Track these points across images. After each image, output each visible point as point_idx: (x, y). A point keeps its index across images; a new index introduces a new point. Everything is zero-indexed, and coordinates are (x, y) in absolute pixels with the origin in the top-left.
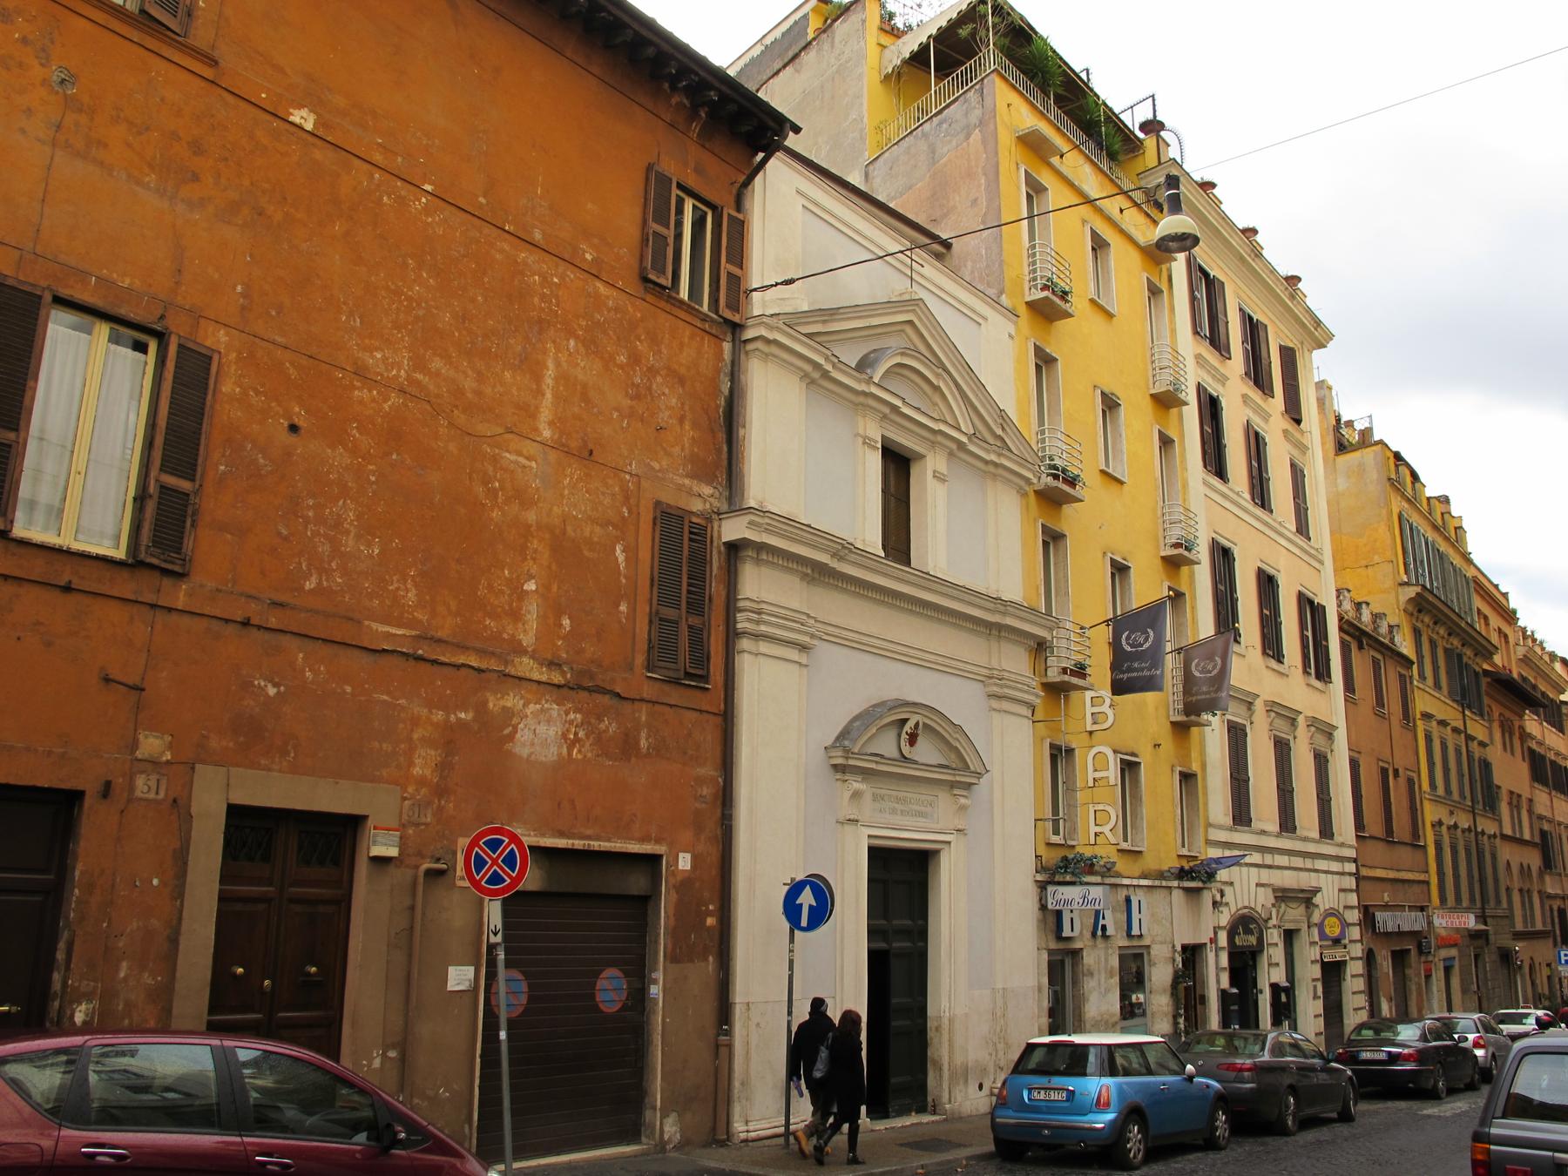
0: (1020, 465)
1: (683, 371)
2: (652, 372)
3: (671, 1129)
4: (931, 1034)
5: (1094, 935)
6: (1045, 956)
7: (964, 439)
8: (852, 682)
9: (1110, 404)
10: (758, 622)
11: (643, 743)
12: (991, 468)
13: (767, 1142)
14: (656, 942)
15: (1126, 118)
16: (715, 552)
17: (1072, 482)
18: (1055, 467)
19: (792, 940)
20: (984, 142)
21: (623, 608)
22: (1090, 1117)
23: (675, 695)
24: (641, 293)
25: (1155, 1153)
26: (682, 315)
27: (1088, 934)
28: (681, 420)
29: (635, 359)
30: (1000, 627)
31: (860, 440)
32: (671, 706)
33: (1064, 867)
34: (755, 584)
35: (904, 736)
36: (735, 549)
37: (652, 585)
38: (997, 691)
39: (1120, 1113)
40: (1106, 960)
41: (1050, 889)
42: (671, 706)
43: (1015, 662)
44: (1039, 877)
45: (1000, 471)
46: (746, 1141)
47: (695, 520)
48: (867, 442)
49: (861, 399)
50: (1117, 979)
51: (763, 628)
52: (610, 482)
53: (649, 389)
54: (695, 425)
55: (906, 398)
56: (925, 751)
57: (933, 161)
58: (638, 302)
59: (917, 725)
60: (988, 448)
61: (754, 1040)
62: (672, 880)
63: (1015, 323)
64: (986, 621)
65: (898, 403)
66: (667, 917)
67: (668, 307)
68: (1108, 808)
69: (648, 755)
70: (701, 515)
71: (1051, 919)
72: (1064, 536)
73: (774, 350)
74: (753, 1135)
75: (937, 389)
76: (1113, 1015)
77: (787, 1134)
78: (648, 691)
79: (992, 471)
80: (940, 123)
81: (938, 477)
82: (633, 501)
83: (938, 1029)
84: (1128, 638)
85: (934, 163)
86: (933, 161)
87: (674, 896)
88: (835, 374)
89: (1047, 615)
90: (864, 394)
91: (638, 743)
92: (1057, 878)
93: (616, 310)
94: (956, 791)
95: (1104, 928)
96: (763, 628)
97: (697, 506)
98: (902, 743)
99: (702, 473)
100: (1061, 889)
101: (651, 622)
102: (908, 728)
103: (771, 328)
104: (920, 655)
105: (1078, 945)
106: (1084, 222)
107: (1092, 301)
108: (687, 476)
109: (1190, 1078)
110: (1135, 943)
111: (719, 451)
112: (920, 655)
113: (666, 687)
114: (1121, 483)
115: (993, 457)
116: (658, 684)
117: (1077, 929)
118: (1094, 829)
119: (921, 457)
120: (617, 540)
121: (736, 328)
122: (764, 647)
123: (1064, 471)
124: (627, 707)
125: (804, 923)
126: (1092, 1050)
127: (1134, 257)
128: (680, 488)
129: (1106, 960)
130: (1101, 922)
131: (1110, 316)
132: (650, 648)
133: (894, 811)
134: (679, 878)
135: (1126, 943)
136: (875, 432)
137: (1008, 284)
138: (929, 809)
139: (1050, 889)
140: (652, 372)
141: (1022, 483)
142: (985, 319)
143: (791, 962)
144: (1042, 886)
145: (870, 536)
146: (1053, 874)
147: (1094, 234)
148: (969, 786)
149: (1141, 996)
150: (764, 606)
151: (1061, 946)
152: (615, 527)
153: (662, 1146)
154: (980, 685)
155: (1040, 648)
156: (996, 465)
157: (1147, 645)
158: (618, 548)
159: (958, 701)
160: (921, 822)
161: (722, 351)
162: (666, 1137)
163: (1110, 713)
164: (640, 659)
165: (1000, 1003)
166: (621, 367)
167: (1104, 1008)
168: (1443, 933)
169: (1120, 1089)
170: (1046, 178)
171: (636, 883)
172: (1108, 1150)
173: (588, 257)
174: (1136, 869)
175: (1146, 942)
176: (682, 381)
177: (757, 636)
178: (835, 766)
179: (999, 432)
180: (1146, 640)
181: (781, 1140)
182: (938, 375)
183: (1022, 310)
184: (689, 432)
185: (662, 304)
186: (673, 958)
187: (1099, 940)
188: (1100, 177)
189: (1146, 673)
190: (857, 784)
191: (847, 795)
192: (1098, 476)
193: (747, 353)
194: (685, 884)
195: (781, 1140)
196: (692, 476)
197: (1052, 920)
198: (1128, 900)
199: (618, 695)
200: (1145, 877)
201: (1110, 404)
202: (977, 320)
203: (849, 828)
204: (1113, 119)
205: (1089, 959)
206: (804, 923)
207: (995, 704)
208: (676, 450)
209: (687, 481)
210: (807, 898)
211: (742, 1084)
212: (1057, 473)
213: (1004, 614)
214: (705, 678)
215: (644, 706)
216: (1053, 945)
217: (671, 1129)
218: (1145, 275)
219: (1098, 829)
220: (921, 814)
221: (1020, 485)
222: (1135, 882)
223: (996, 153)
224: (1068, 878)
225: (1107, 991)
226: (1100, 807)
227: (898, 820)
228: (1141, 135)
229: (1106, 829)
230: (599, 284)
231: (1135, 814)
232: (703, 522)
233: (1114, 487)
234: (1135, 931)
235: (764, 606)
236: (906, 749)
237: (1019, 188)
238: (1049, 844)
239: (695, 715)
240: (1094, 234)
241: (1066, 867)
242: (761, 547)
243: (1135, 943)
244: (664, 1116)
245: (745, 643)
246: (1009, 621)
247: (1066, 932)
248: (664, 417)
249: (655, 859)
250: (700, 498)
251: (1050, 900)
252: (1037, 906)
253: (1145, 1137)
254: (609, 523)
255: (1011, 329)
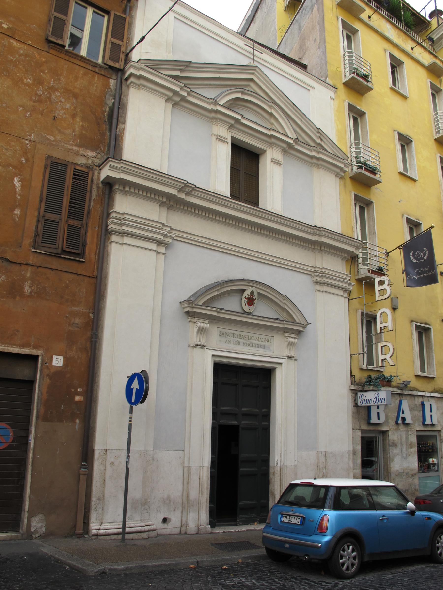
0: (334, 159)
1: (76, 91)
2: (52, 89)
3: (38, 524)
4: (271, 476)
5: (397, 423)
6: (359, 434)
7: (291, 141)
8: (201, 266)
9: (405, 142)
10: (121, 225)
11: (27, 289)
12: (314, 161)
13: (108, 537)
14: (33, 409)
15: (422, 14)
16: (94, 187)
17: (373, 171)
18: (360, 162)
19: (131, 411)
20: (318, 10)
21: (17, 212)
22: (315, 538)
23: (55, 263)
24: (46, 48)
25: (365, 567)
26: (78, 62)
27: (392, 422)
28: (74, 116)
29: (39, 82)
30: (321, 244)
31: (214, 138)
32: (52, 269)
33: (369, 379)
34: (123, 205)
35: (244, 299)
36: (109, 185)
37: (41, 201)
38: (321, 280)
39: (334, 536)
40: (407, 438)
41: (359, 394)
42: (52, 269)
43: (336, 266)
44: (353, 388)
45: (321, 162)
46: (97, 535)
47: (78, 168)
48: (220, 139)
49: (213, 115)
50: (415, 449)
51: (124, 228)
52: (13, 144)
53: (50, 98)
54: (84, 119)
55: (249, 118)
56: (262, 310)
57: (300, 31)
58: (44, 53)
59: (252, 293)
60: (309, 149)
61: (109, 472)
62: (46, 371)
63: (336, 92)
64: (314, 240)
65: (239, 117)
66: (40, 393)
67: (67, 58)
68: (388, 344)
69: (30, 296)
70: (85, 166)
71: (364, 413)
72: (372, 202)
73: (142, 82)
74: (101, 532)
75: (271, 114)
76: (413, 470)
77: (124, 533)
78: (32, 259)
79: (315, 162)
80: (302, 12)
81: (274, 161)
82: (29, 155)
83: (274, 473)
84: (414, 255)
85: (300, 32)
86: (300, 31)
87: (47, 381)
88: (190, 99)
89: (363, 245)
90: (212, 111)
91: (23, 288)
92: (366, 388)
93: (26, 55)
94: (286, 335)
95: (404, 419)
96: (124, 228)
97: (82, 161)
98: (243, 304)
99: (86, 142)
100: (365, 394)
101: (38, 221)
102: (246, 294)
103: (138, 69)
104: (257, 255)
105: (385, 428)
106: (385, 50)
107: (391, 88)
108: (76, 145)
109: (412, 513)
110: (429, 429)
111: (103, 134)
112: (257, 255)
113: (49, 259)
114: (415, 181)
115: (314, 154)
116: (42, 257)
117: (380, 417)
118: (381, 357)
119: (265, 151)
120: (16, 175)
121: (122, 71)
122: (127, 240)
123: (365, 164)
124: (16, 268)
125: (133, 401)
126: (332, 488)
127: (422, 74)
128: (69, 151)
129: (407, 438)
130: (401, 415)
131: (405, 97)
132: (37, 235)
133: (238, 343)
134: (52, 371)
135: (422, 428)
136: (228, 135)
137: (329, 73)
138: (266, 344)
139: (359, 394)
140: (52, 89)
141: (338, 170)
142: (313, 88)
143: (130, 425)
144: (355, 393)
145: (222, 184)
146: (363, 386)
147: (392, 57)
148: (299, 333)
149: (435, 460)
150: (126, 216)
151: (371, 428)
152: (14, 167)
153: (29, 535)
154: (309, 277)
155: (353, 259)
156: (318, 159)
157: (426, 258)
158: (16, 180)
159: (293, 286)
160: (260, 351)
161: (108, 84)
162: (33, 529)
163: (388, 288)
164: (27, 242)
165: (322, 459)
166: (28, 85)
167: (405, 465)
168: (114, 76)
169: (340, 519)
170: (357, 26)
171: (21, 372)
172: (325, 564)
173: (5, 26)
174: (430, 386)
175: (438, 428)
176: (76, 96)
177: (123, 234)
178: (188, 313)
179: (319, 141)
180: (424, 254)
181: (120, 537)
182: (271, 107)
183: (341, 87)
184: (78, 122)
185: (62, 56)
186: (44, 418)
187: (402, 427)
188: (397, 31)
189: (428, 274)
190: (201, 324)
191: (196, 330)
192: (398, 176)
193: (128, 86)
194: (58, 374)
195: (120, 537)
196: (80, 146)
197: (362, 412)
198: (423, 404)
199: (8, 260)
200: (436, 392)
201: (405, 142)
202: (307, 88)
203: (198, 351)
204: (416, 15)
205: (393, 436)
206: (133, 401)
207: (318, 287)
208: (69, 131)
209: (75, 148)
210: (135, 385)
211: (99, 499)
212: (362, 165)
213: (320, 236)
214: (82, 255)
215: (30, 269)
216: (365, 427)
217: (38, 524)
218: (429, 80)
219: (383, 357)
220: (263, 347)
221: (340, 174)
222: (428, 394)
223: (323, 11)
224: (371, 388)
225: (408, 455)
226: (384, 344)
227: (241, 348)
228: (429, 20)
229: (387, 357)
230: (12, 41)
231: (429, 357)
232: (86, 170)
233: (410, 184)
234: (428, 421)
235: (126, 216)
236: (246, 308)
237: (338, 28)
238: (362, 369)
239: (71, 276)
240: (392, 57)
241: (370, 382)
242: (124, 183)
243: (429, 429)
244: (32, 515)
245: (114, 238)
246: (324, 240)
247: (374, 420)
248: (59, 113)
249: (35, 358)
250: (85, 157)
251: (359, 401)
252: (353, 404)
253: (361, 555)
254: (9, 165)
255: (333, 95)
